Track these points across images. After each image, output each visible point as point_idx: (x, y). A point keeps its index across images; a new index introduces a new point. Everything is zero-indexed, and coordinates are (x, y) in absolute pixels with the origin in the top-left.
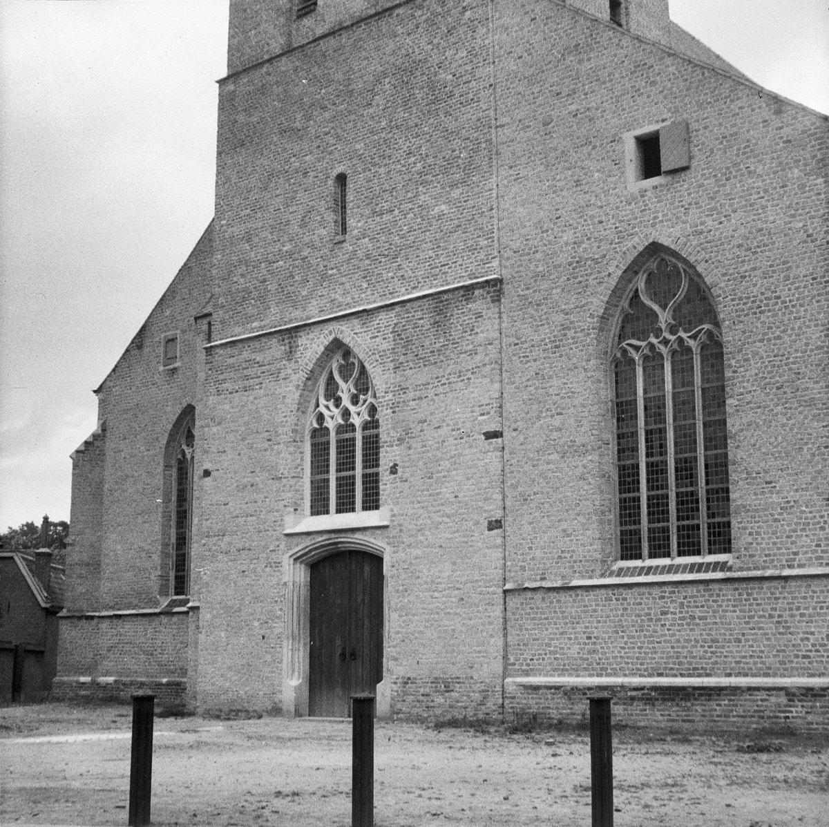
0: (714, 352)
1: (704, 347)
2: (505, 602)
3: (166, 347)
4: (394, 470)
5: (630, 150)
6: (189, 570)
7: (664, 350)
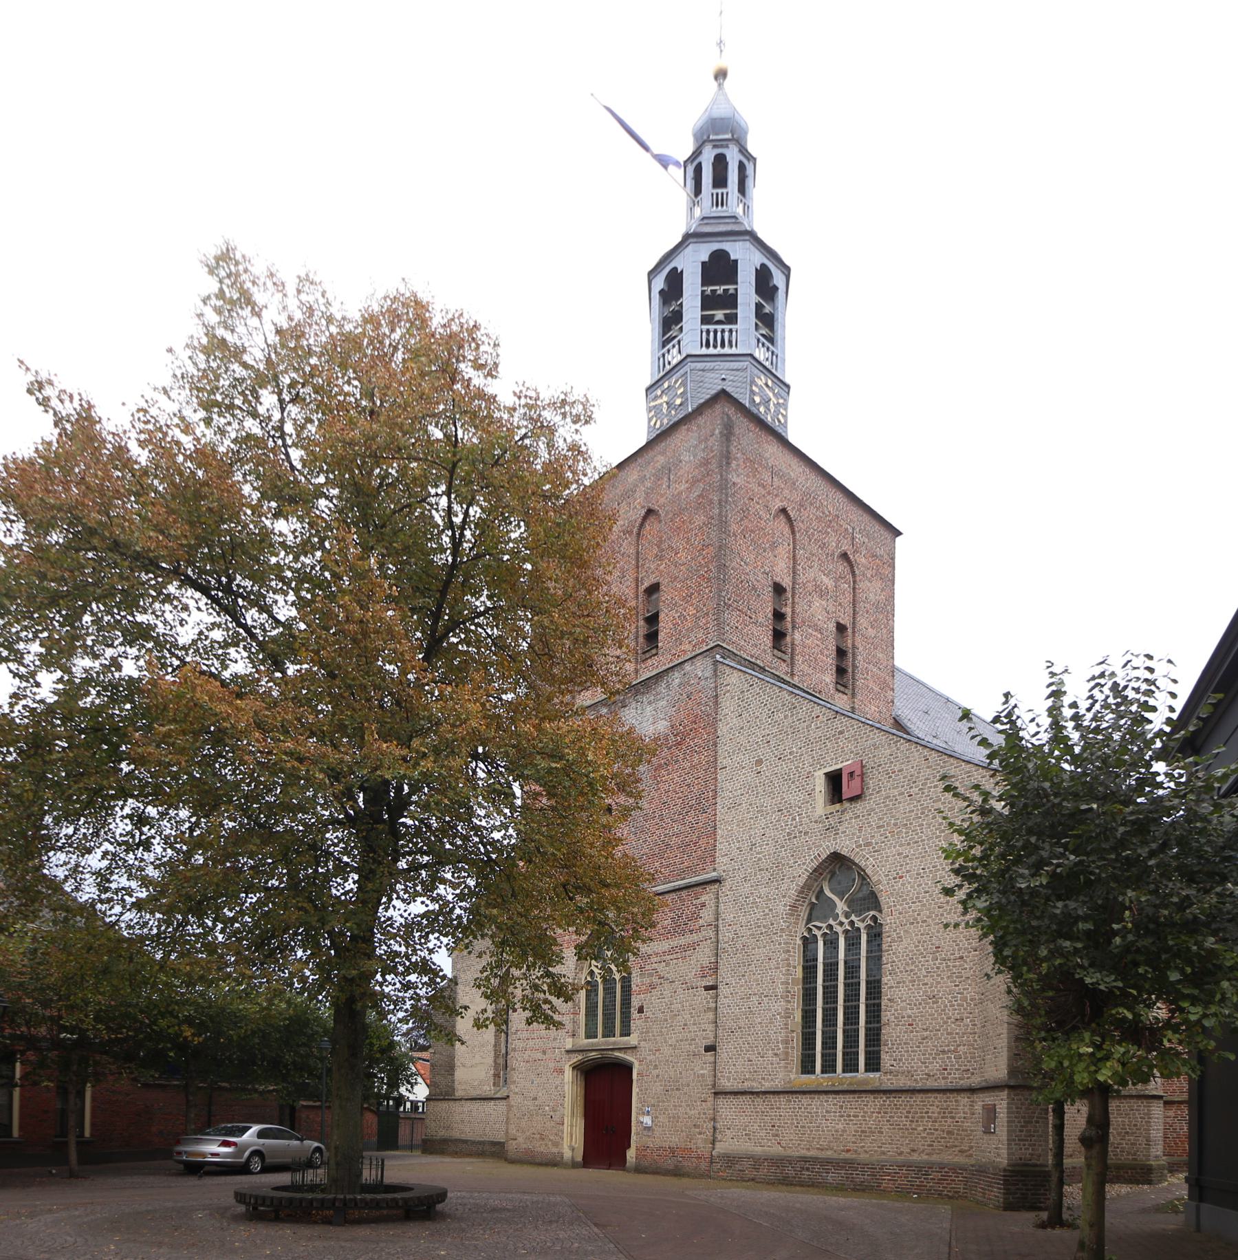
0: (876, 934)
1: (868, 927)
2: (461, 1099)
3: (863, 792)
4: (641, 1010)
5: (820, 784)
6: (1009, 1048)
7: (839, 929)
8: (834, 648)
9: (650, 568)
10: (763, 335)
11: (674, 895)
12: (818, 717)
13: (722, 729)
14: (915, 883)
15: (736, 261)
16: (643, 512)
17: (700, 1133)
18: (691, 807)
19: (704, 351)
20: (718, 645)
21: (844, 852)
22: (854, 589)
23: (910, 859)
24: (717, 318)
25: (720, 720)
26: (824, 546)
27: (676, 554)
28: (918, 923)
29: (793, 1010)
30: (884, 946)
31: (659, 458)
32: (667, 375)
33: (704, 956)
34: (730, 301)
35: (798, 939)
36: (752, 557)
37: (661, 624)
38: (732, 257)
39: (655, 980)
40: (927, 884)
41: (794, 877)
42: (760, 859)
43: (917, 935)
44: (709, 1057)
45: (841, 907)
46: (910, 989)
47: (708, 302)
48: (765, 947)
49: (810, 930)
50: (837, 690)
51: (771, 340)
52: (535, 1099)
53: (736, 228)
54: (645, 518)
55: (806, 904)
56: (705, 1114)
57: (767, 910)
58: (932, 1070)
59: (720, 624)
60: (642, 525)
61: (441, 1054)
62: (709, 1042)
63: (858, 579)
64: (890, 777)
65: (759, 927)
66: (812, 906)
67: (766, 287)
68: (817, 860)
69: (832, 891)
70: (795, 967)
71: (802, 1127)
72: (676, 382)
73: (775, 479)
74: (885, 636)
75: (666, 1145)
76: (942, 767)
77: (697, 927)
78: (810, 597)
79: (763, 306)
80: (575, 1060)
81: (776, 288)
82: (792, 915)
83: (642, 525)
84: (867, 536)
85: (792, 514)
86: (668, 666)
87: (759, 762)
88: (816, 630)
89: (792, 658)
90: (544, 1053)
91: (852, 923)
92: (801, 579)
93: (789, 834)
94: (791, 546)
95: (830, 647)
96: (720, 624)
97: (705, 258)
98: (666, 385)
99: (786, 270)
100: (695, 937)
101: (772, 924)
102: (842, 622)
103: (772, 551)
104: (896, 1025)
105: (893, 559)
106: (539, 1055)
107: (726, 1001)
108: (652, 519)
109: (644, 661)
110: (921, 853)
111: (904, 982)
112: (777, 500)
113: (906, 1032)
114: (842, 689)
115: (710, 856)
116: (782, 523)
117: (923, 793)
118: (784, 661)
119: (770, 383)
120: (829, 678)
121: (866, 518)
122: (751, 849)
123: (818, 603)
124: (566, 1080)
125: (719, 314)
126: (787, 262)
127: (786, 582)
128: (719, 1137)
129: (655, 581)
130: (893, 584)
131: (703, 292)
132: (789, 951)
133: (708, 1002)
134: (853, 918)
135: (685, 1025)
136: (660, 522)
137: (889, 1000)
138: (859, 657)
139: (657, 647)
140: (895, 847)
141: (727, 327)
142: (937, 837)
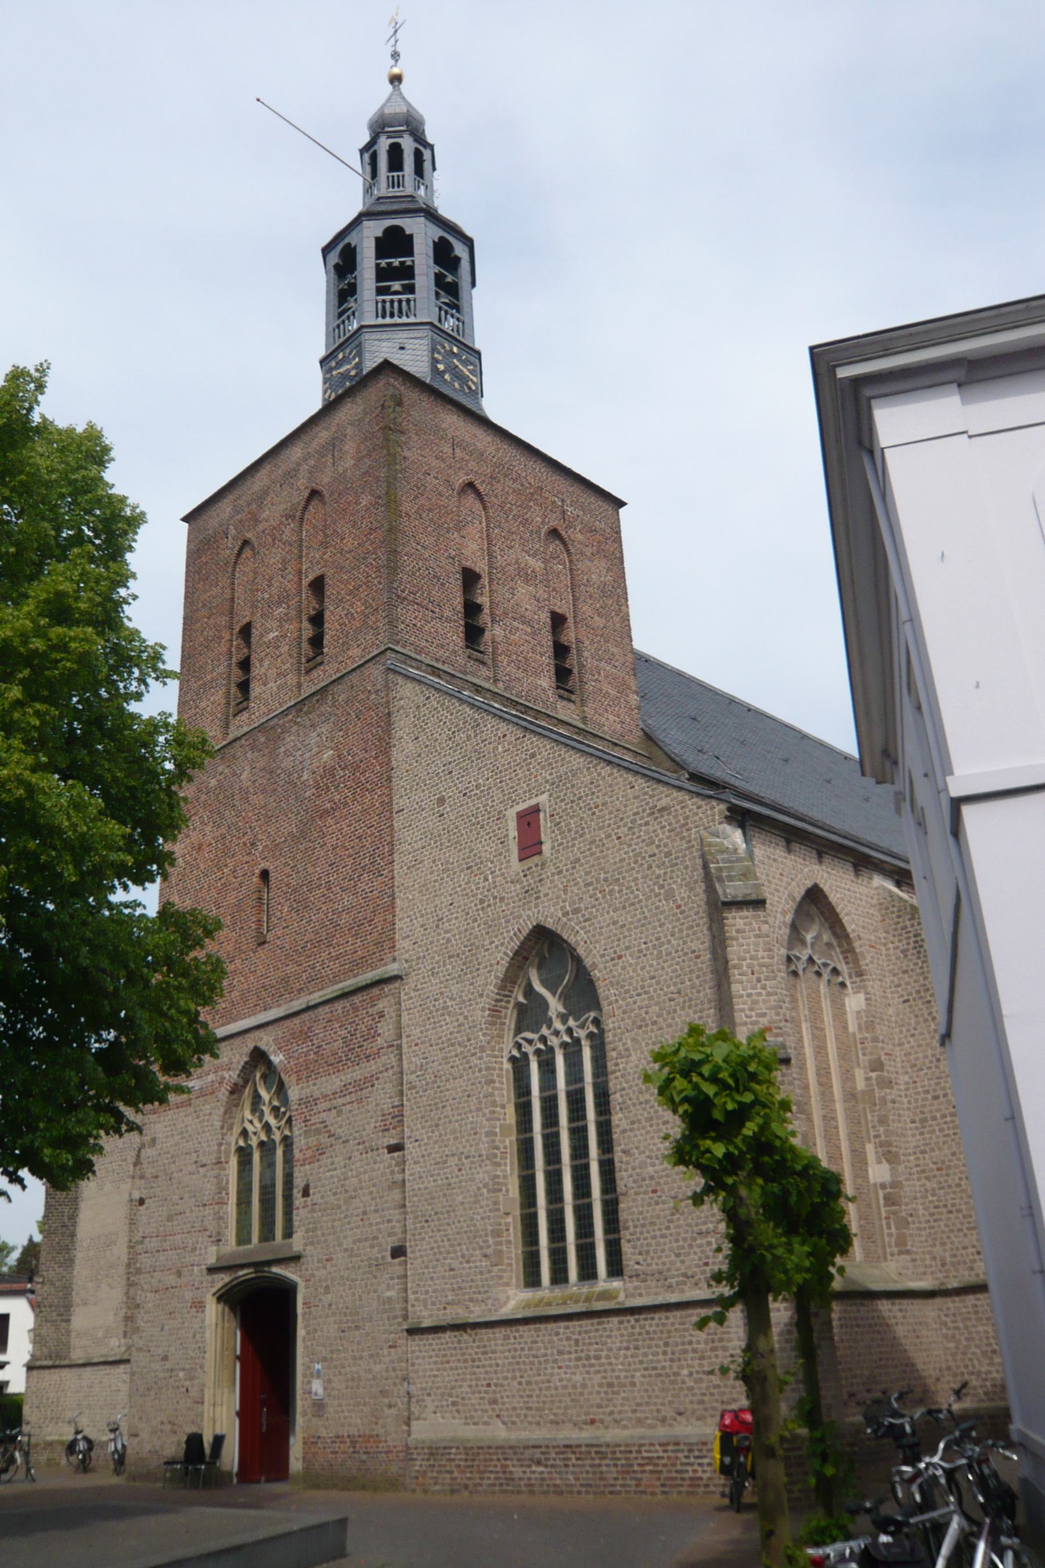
0: (598, 1042)
4: (306, 1193)
7: (554, 1041)
8: (550, 643)
9: (314, 557)
10: (444, 303)
11: (345, 1003)
12: (505, 736)
13: (397, 756)
14: (637, 964)
15: (411, 236)
16: (306, 494)
17: (390, 1406)
18: (363, 868)
19: (380, 321)
20: (389, 649)
21: (550, 924)
22: (571, 570)
23: (630, 930)
24: (393, 289)
25: (394, 746)
26: (525, 522)
27: (342, 540)
28: (647, 1025)
29: (505, 1177)
30: (609, 1064)
31: (322, 435)
32: (340, 347)
33: (382, 1096)
34: (408, 272)
35: (505, 1060)
36: (432, 539)
37: (326, 625)
38: (407, 232)
39: (324, 1139)
40: (651, 966)
41: (491, 965)
42: (449, 940)
43: (647, 1044)
44: (396, 1266)
45: (555, 1005)
46: (648, 1132)
47: (382, 274)
48: (461, 1077)
49: (519, 1046)
50: (560, 697)
51: (458, 308)
52: (165, 1358)
53: (411, 206)
54: (309, 500)
55: (511, 1005)
56: (394, 1370)
57: (461, 1018)
58: (690, 1267)
59: (392, 623)
60: (305, 508)
61: (52, 1284)
62: (392, 1242)
63: (574, 558)
64: (594, 813)
65: (452, 1045)
66: (520, 1008)
67: (444, 255)
68: (518, 938)
69: (544, 983)
70: (503, 1107)
71: (528, 1383)
72: (350, 354)
73: (457, 450)
74: (618, 625)
75: (344, 1431)
76: (651, 797)
77: (375, 1049)
78: (511, 583)
79: (446, 276)
80: (220, 1285)
81: (458, 260)
82: (493, 1024)
83: (305, 508)
84: (583, 509)
85: (481, 488)
86: (334, 677)
87: (441, 801)
88: (524, 623)
89: (494, 660)
90: (179, 1274)
91: (570, 1031)
92: (500, 561)
93: (482, 901)
94: (484, 524)
95: (543, 642)
96: (392, 623)
97: (380, 234)
98: (341, 356)
99: (469, 242)
100: (372, 1067)
101: (469, 1040)
102: (559, 611)
103: (459, 530)
104: (637, 1194)
105: (618, 532)
106: (171, 1279)
107: (417, 1168)
108: (315, 502)
109: (308, 672)
110: (639, 920)
111: (639, 1121)
112: (460, 473)
113: (649, 1205)
114: (566, 694)
115: (386, 942)
116: (471, 499)
117: (634, 834)
118: (483, 663)
119: (455, 350)
120: (546, 682)
121: (576, 489)
122: (437, 926)
123: (523, 591)
124: (207, 1322)
125: (396, 286)
126: (469, 232)
127: (480, 566)
128: (415, 1409)
129: (318, 573)
130: (622, 563)
131: (378, 265)
132: (493, 1081)
133: (393, 1172)
134: (571, 1023)
135: (365, 1213)
136: (324, 504)
137: (624, 1152)
138: (585, 654)
139: (322, 653)
140: (608, 913)
141: (403, 297)
142: (656, 896)
